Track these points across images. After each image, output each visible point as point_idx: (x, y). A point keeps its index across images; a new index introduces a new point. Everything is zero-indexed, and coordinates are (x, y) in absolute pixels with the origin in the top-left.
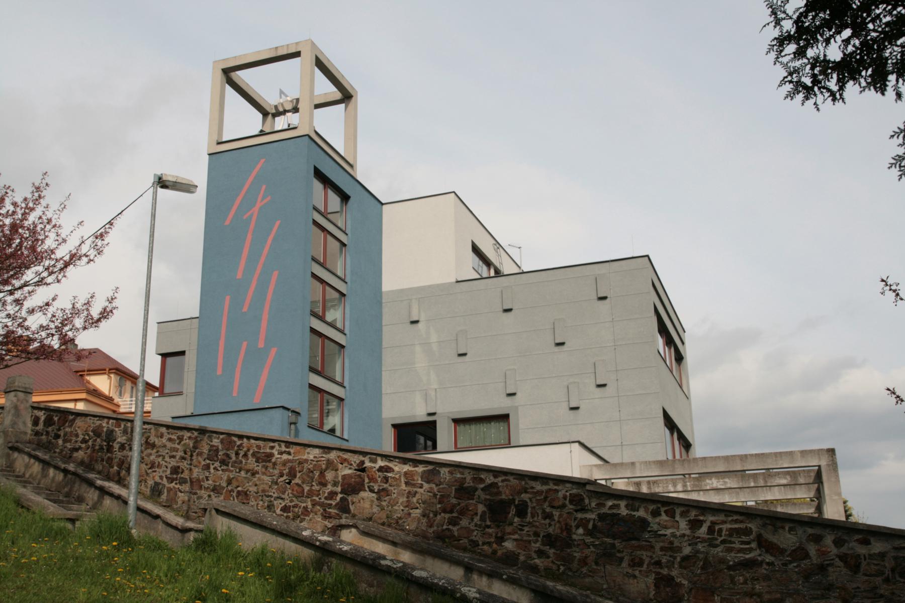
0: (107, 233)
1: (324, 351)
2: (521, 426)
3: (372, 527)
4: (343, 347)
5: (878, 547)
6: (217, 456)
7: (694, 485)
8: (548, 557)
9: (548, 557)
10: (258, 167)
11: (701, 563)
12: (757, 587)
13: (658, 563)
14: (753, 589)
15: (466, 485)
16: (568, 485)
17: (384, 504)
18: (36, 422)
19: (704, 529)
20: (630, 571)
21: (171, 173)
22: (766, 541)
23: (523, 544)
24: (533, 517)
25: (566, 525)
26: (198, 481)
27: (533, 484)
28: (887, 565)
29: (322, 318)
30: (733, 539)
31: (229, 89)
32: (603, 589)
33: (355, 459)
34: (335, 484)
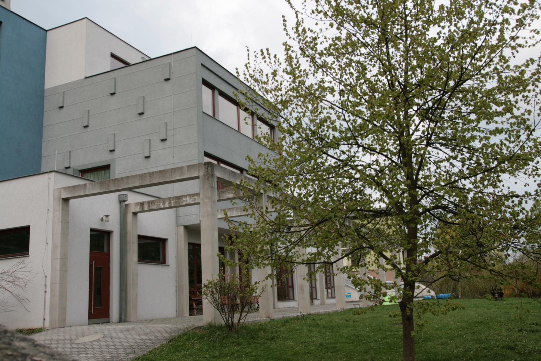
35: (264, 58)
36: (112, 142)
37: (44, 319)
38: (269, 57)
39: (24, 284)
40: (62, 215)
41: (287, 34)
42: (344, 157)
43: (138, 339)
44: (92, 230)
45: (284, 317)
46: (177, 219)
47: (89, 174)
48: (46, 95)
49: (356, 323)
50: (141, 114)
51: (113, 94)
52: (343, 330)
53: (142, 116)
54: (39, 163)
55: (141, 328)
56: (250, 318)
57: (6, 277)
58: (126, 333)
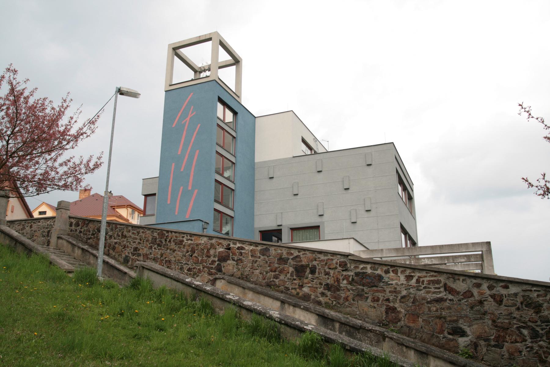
0: (96, 121)
1: (223, 193)
2: (326, 232)
3: (232, 279)
4: (233, 190)
5: (513, 289)
6: (156, 242)
8: (327, 296)
9: (327, 296)
10: (190, 97)
11: (412, 300)
12: (443, 313)
13: (388, 300)
14: (441, 314)
15: (283, 257)
16: (339, 256)
17: (240, 267)
18: (71, 225)
19: (414, 280)
20: (372, 304)
21: (125, 87)
22: (449, 287)
23: (314, 289)
24: (319, 274)
25: (337, 278)
26: (147, 255)
27: (319, 256)
28: (518, 300)
29: (222, 175)
30: (430, 286)
31: (176, 59)
32: (357, 314)
33: (225, 243)
34: (215, 257)
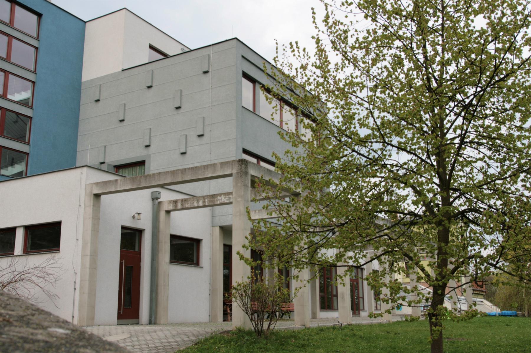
7: (210, 201)
35: (293, 51)
36: (148, 137)
37: (73, 317)
38: (298, 51)
39: (54, 280)
40: (93, 211)
41: (316, 27)
42: (372, 155)
43: (164, 340)
44: (123, 228)
45: (319, 327)
46: (212, 219)
47: (124, 170)
48: (83, 87)
49: (397, 335)
50: (178, 108)
51: (149, 87)
52: (381, 341)
53: (178, 110)
54: (74, 157)
55: (168, 330)
56: (280, 326)
57: (37, 272)
58: (153, 334)
